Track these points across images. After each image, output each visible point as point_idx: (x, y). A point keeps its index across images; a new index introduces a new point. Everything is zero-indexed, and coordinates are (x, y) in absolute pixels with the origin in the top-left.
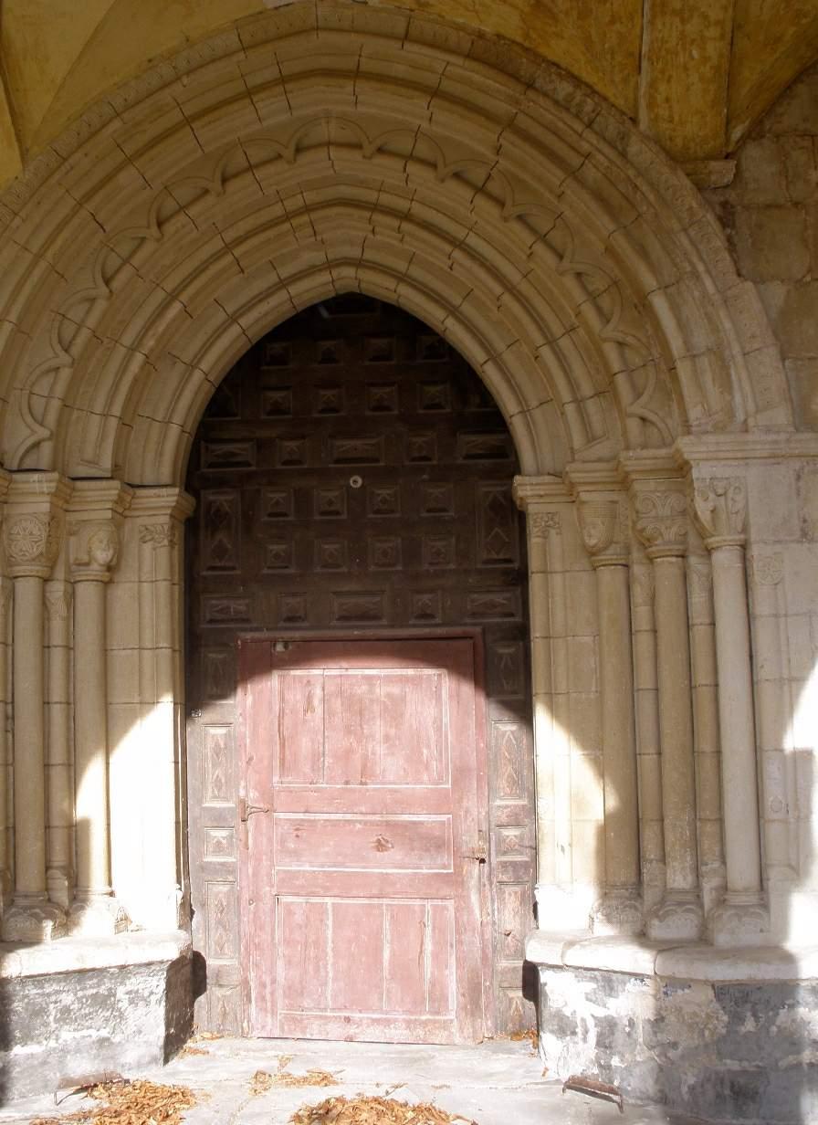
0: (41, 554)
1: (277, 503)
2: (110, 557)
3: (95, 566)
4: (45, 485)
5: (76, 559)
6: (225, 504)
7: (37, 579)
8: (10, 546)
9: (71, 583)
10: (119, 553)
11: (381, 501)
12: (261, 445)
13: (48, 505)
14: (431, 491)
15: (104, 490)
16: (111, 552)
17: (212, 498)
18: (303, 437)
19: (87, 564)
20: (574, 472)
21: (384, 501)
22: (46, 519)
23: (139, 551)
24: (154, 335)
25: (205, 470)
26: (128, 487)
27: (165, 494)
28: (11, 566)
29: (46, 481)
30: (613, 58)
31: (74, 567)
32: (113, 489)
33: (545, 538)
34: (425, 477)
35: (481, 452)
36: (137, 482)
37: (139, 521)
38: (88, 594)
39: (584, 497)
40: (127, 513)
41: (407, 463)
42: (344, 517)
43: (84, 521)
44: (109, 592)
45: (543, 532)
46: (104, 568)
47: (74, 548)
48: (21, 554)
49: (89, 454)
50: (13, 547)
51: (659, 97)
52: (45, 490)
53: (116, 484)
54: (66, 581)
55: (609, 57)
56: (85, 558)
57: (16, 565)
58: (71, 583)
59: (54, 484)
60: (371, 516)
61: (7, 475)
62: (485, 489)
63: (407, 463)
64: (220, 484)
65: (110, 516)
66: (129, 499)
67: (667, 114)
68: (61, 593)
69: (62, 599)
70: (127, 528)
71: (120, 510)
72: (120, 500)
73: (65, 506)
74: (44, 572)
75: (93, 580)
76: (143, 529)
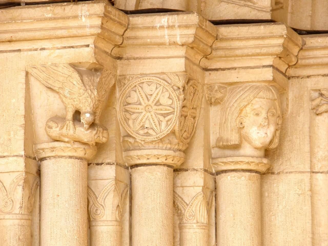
0: (173, 132)
2: (270, 135)
3: (247, 150)
4: (178, 32)
5: (219, 140)
7: (166, 168)
8: (127, 120)
9: (212, 174)
10: (282, 132)
13: (183, 61)
15: (263, 38)
16: (272, 128)
19: (236, 147)
22: (180, 83)
23: (311, 127)
26: (295, 34)
27: (166, 24)
28: (127, 150)
29: (180, 27)
31: (215, 152)
32: (274, 37)
36: (306, 25)
37: (310, 83)
38: (237, 190)
40: (291, 72)
43: (231, 84)
44: (266, 187)
46: (262, 153)
47: (217, 124)
48: (141, 132)
50: (130, 122)
52: (179, 40)
53: (280, 29)
54: (206, 171)
56: (234, 139)
57: (134, 149)
58: (212, 174)
59: (192, 31)
61: (123, 18)
65: (271, 78)
66: (295, 50)
68: (200, 189)
69: (201, 197)
70: (291, 95)
71: (283, 68)
72: (284, 55)
73: (205, 63)
74: (174, 158)
75: (244, 171)
76: (316, 94)
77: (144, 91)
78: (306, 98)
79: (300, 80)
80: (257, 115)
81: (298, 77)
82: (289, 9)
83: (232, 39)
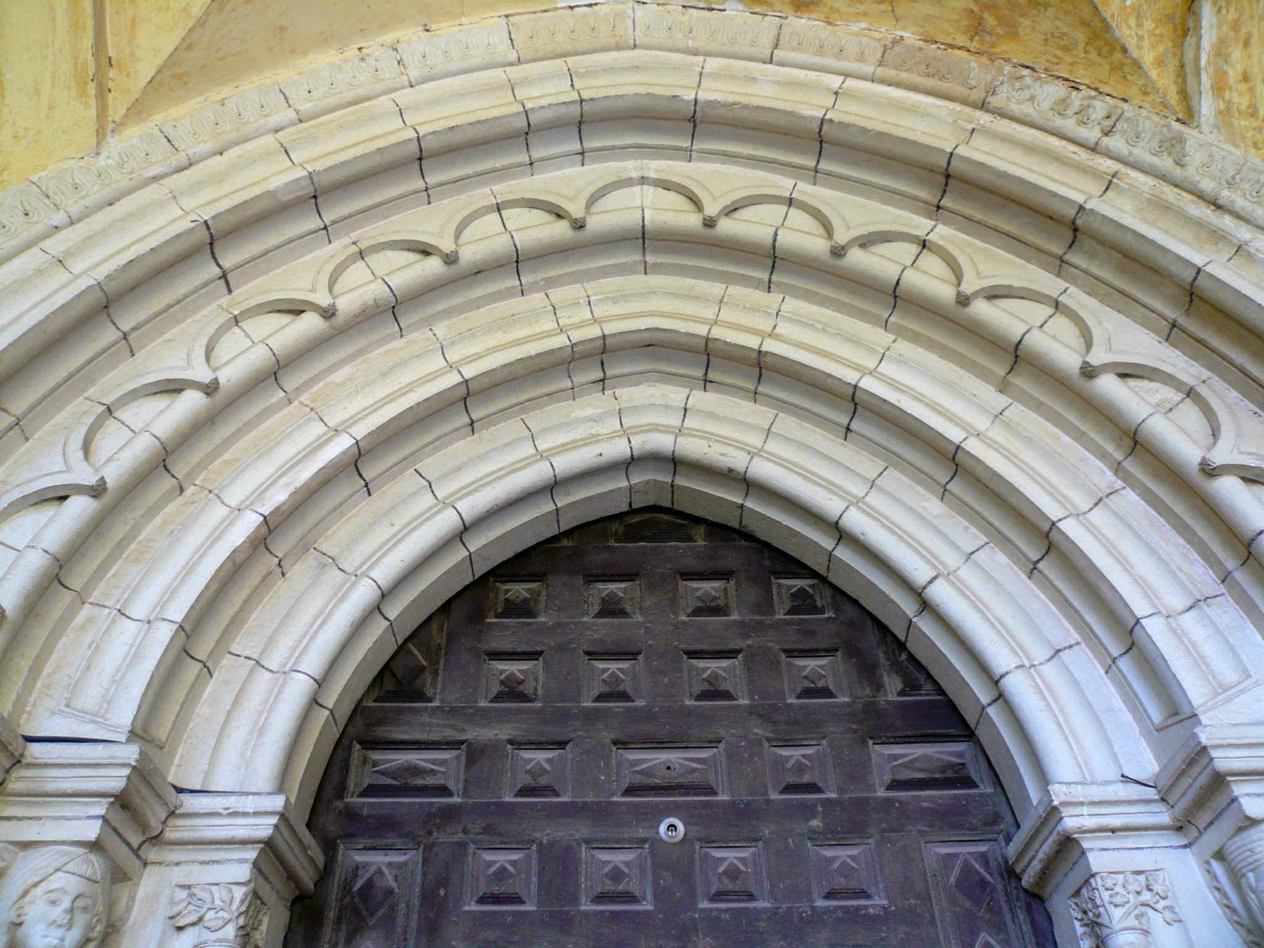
1: (502, 874)
6: (386, 871)
11: (726, 873)
12: (475, 754)
14: (829, 853)
17: (359, 858)
18: (562, 744)
20: (1221, 746)
21: (733, 873)
24: (288, 485)
25: (353, 800)
30: (1139, 25)
33: (1146, 932)
34: (815, 823)
35: (922, 775)
37: (178, 875)
39: (1252, 807)
41: (774, 796)
42: (647, 906)
45: (1137, 917)
49: (90, 697)
51: (1230, 71)
55: (1132, 22)
60: (705, 905)
62: (944, 850)
63: (774, 796)
64: (382, 829)
67: (1244, 102)
77: (179, 585)
78: (164, 899)
79: (163, 868)
80: (53, 903)
81: (161, 864)
82: (177, 760)
83: (46, 765)
